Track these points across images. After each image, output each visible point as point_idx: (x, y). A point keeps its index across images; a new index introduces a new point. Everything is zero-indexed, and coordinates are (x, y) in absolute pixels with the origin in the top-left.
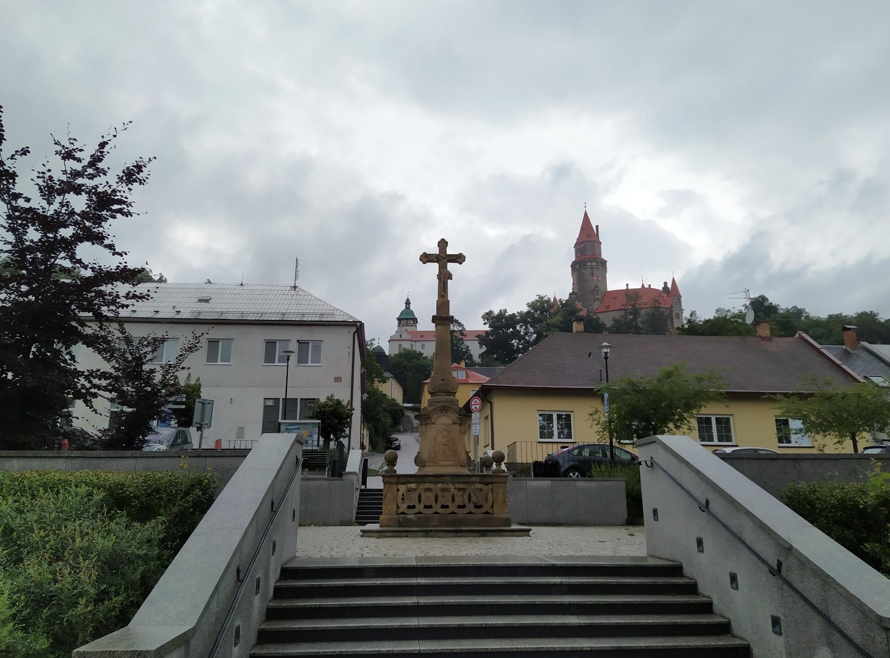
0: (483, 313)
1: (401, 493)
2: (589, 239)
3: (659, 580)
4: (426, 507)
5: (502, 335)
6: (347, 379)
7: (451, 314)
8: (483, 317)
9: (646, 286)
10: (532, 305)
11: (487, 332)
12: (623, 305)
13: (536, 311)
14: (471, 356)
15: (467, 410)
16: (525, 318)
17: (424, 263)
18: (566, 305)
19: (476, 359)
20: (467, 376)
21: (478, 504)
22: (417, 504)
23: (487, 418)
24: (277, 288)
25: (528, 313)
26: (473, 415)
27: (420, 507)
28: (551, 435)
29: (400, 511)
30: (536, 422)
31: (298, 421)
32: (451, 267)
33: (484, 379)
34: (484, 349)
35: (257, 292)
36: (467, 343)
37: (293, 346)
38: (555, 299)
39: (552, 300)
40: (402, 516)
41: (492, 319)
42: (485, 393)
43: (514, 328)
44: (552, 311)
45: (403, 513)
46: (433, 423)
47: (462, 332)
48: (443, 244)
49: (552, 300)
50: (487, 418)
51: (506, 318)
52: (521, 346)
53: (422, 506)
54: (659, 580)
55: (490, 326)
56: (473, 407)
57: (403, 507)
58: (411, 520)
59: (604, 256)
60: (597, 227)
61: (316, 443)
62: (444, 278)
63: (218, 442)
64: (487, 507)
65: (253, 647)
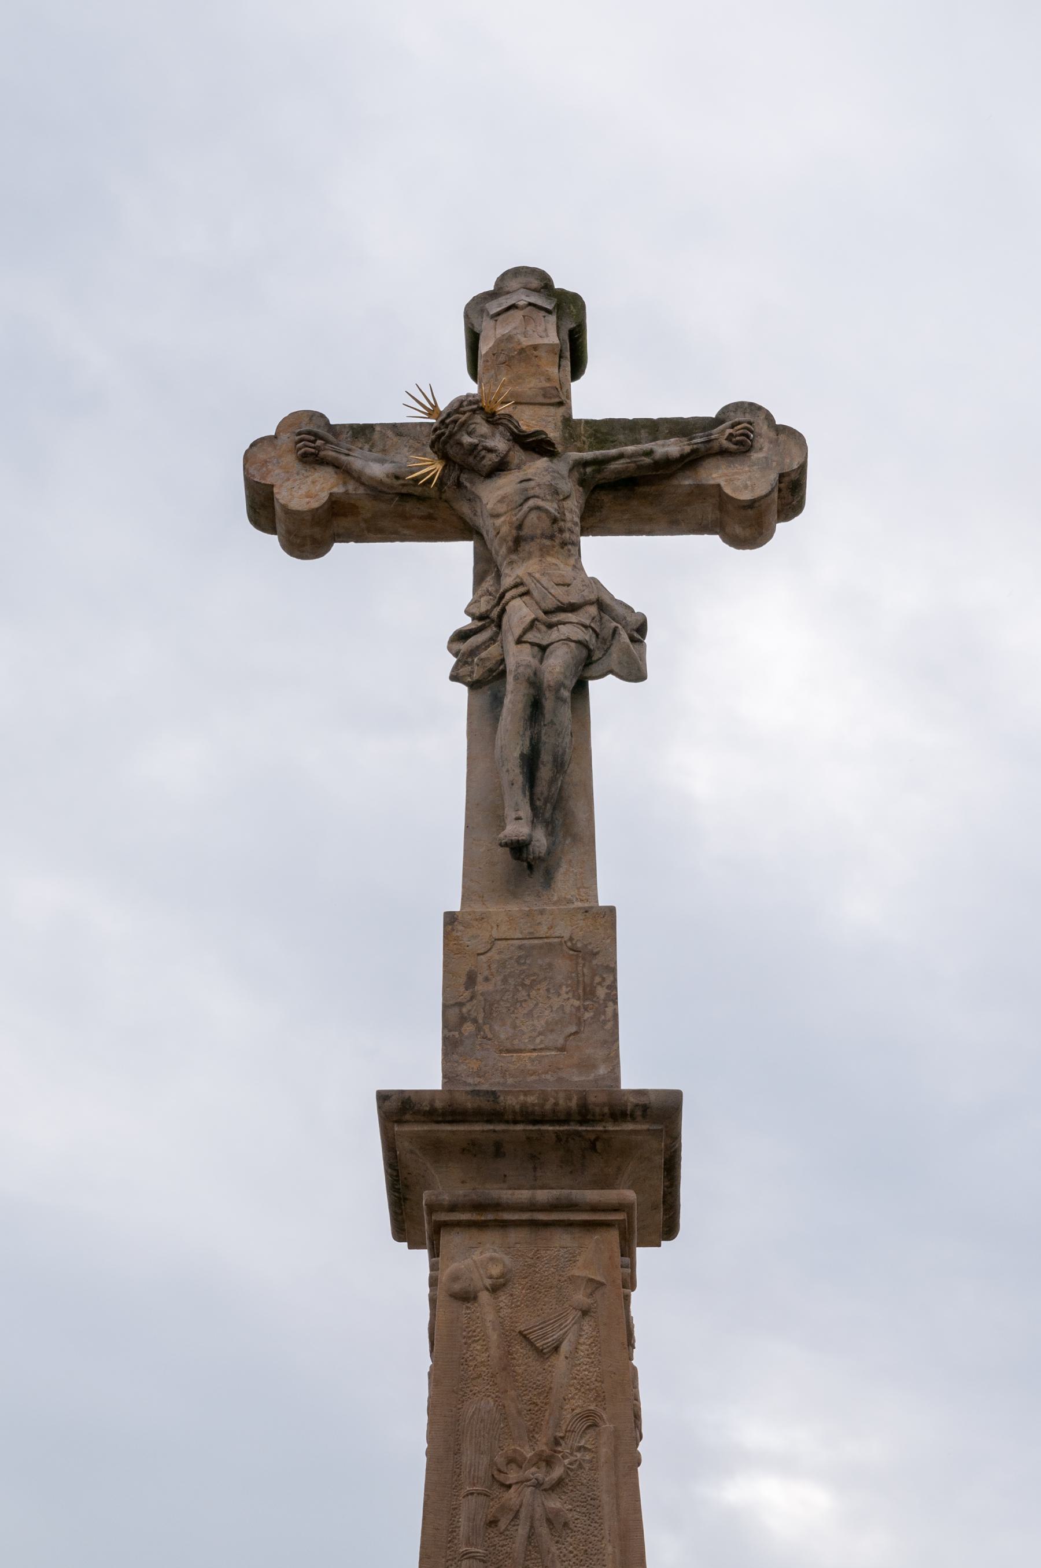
32: (616, 562)
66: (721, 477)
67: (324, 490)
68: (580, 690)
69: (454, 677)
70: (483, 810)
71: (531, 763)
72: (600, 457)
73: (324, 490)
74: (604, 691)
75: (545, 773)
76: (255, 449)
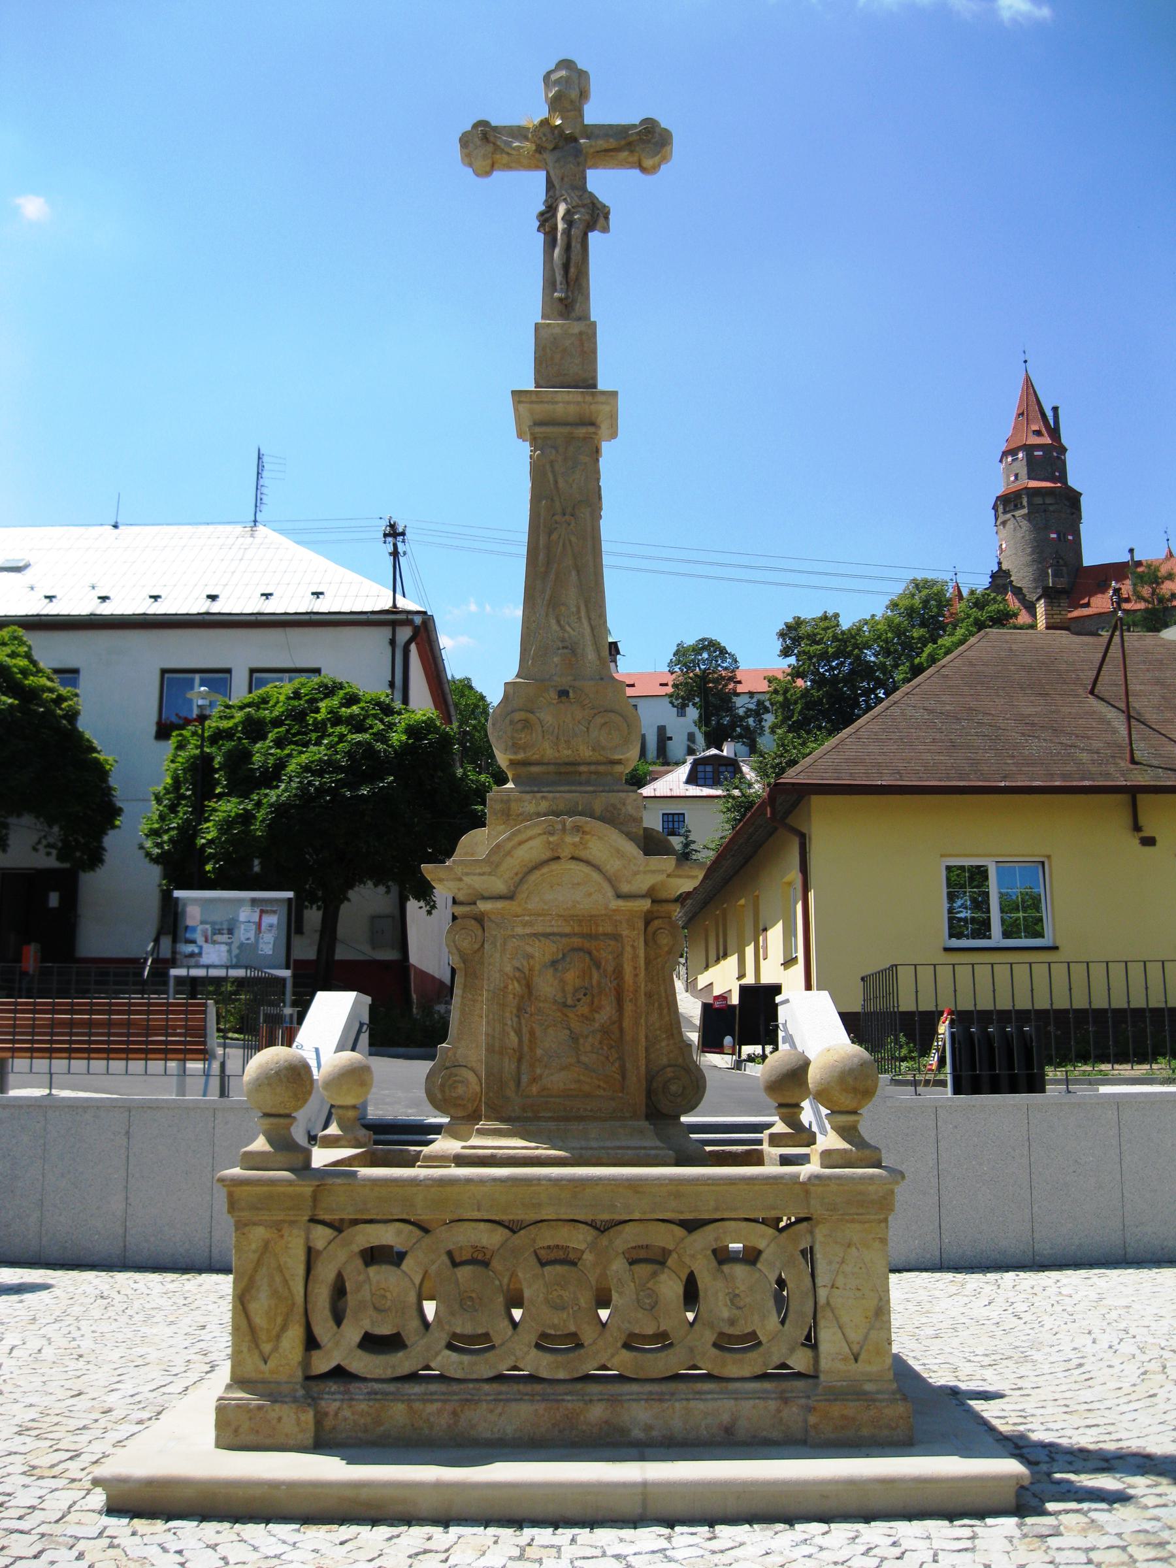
1: (326, 1274)
3: (396, 1137)
7: (592, 319)
29: (322, 1364)
32: (603, 182)
48: (568, 87)
53: (352, 1334)
54: (396, 1137)
60: (1055, 410)
65: (858, 1121)
66: (643, 143)
67: (486, 145)
68: (585, 235)
69: (539, 230)
70: (550, 284)
71: (566, 267)
72: (422, 1177)
73: (486, 145)
74: (594, 237)
75: (572, 270)
76: (604, 1161)
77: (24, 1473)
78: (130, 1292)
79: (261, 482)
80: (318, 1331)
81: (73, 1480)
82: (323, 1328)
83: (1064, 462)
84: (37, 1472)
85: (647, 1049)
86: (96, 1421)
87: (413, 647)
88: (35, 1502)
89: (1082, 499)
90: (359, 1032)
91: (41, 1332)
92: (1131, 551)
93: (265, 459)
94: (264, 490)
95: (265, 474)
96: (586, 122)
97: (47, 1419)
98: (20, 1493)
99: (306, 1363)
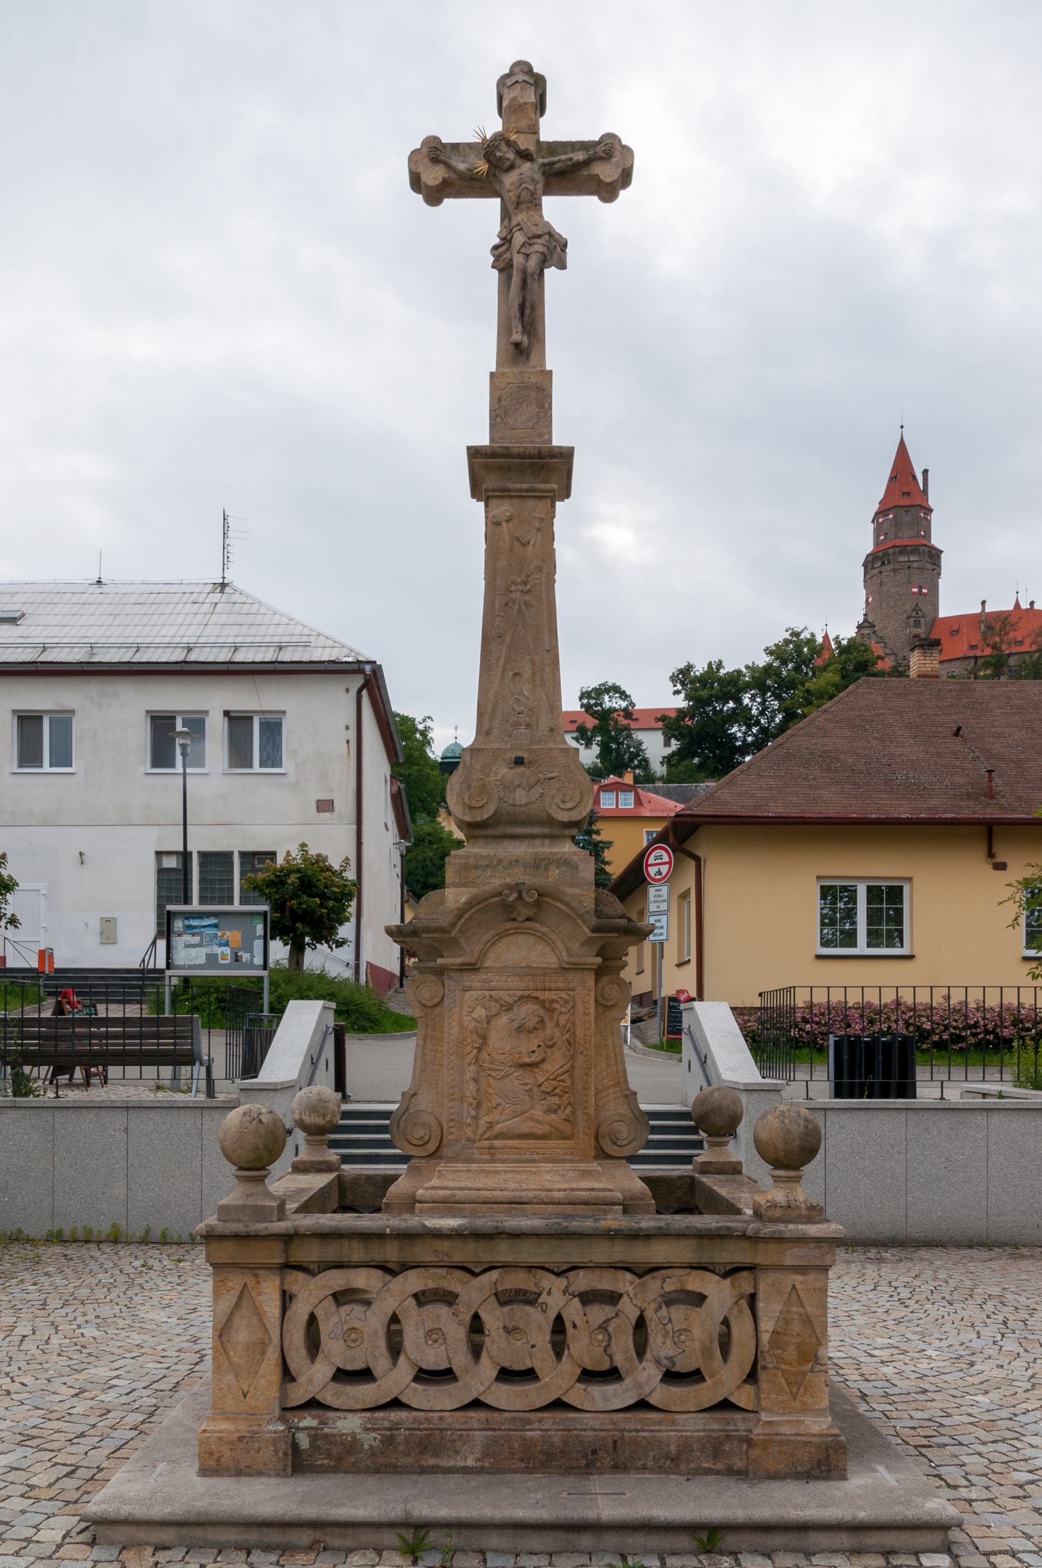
0: (672, 670)
1: (300, 1311)
2: (906, 501)
4: (425, 1376)
5: (712, 721)
6: (345, 804)
8: (673, 679)
9: (1025, 605)
10: (777, 652)
11: (680, 711)
12: (973, 647)
13: (784, 662)
14: (646, 761)
15: (634, 881)
16: (761, 680)
17: (434, 196)
18: (848, 649)
19: (658, 769)
20: (638, 802)
21: (683, 1366)
22: (380, 1364)
23: (684, 896)
24: (182, 589)
25: (768, 669)
26: (652, 891)
27: (396, 1379)
28: (850, 938)
29: (299, 1394)
30: (811, 907)
31: (237, 906)
32: (558, 210)
33: (673, 807)
34: (675, 745)
35: (133, 599)
36: (639, 736)
37: (216, 728)
38: (826, 637)
39: (819, 640)
40: (309, 1421)
41: (692, 682)
42: (681, 835)
43: (738, 701)
44: (818, 662)
45: (313, 1404)
46: (472, 968)
47: (628, 713)
49: (819, 640)
50: (684, 896)
51: (720, 680)
52: (750, 739)
55: (687, 698)
56: (652, 871)
57: (315, 1378)
58: (352, 1445)
59: (936, 541)
60: (925, 472)
61: (258, 960)
62: (525, 265)
63: (45, 955)
64: (726, 1379)
70: (504, 329)
74: (551, 274)
75: (527, 312)
77: (22, 1496)
78: (131, 1270)
79: (227, 542)
80: (293, 1367)
81: (68, 1503)
82: (298, 1357)
83: (929, 522)
84: (35, 1493)
85: (596, 1095)
86: (94, 1426)
87: (365, 693)
88: (29, 1533)
89: (943, 556)
90: (325, 1037)
91: (51, 1319)
92: (984, 603)
93: (230, 520)
94: (230, 549)
95: (230, 534)
96: (542, 139)
97: (49, 1425)
98: (19, 1521)
99: (284, 1395)
